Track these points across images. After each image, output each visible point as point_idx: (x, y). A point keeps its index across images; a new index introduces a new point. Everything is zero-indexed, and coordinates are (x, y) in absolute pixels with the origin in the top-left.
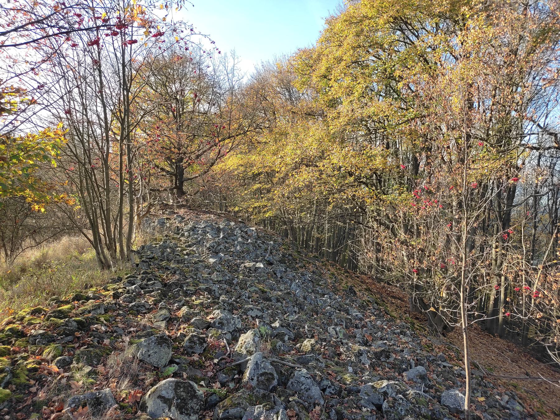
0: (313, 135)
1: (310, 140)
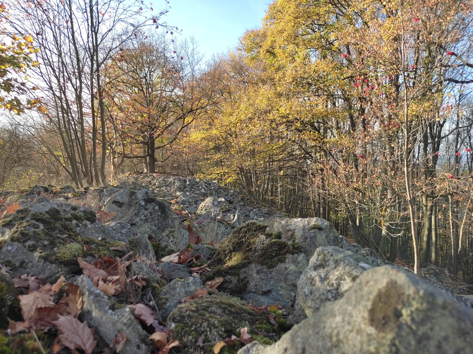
0: (263, 96)
1: (260, 98)
